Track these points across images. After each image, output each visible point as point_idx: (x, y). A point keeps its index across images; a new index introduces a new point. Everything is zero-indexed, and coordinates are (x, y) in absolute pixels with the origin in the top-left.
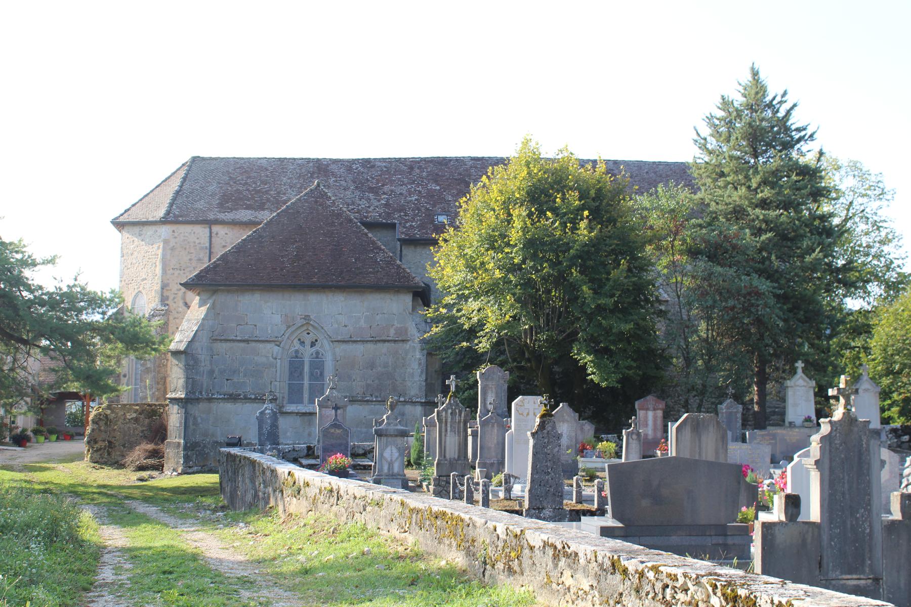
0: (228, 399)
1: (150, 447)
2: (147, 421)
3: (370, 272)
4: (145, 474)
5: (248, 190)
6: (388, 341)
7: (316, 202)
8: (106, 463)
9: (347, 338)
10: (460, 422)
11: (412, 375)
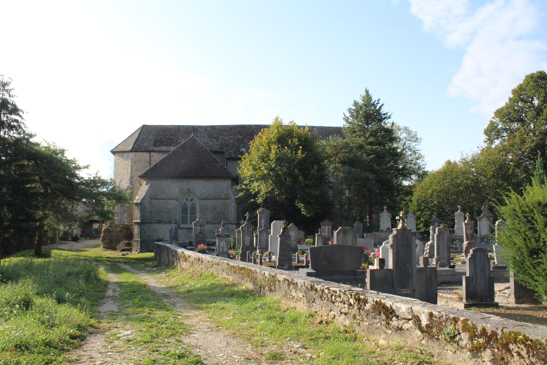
1: (126, 242)
2: (125, 231)
4: (125, 253)
9: (205, 197)
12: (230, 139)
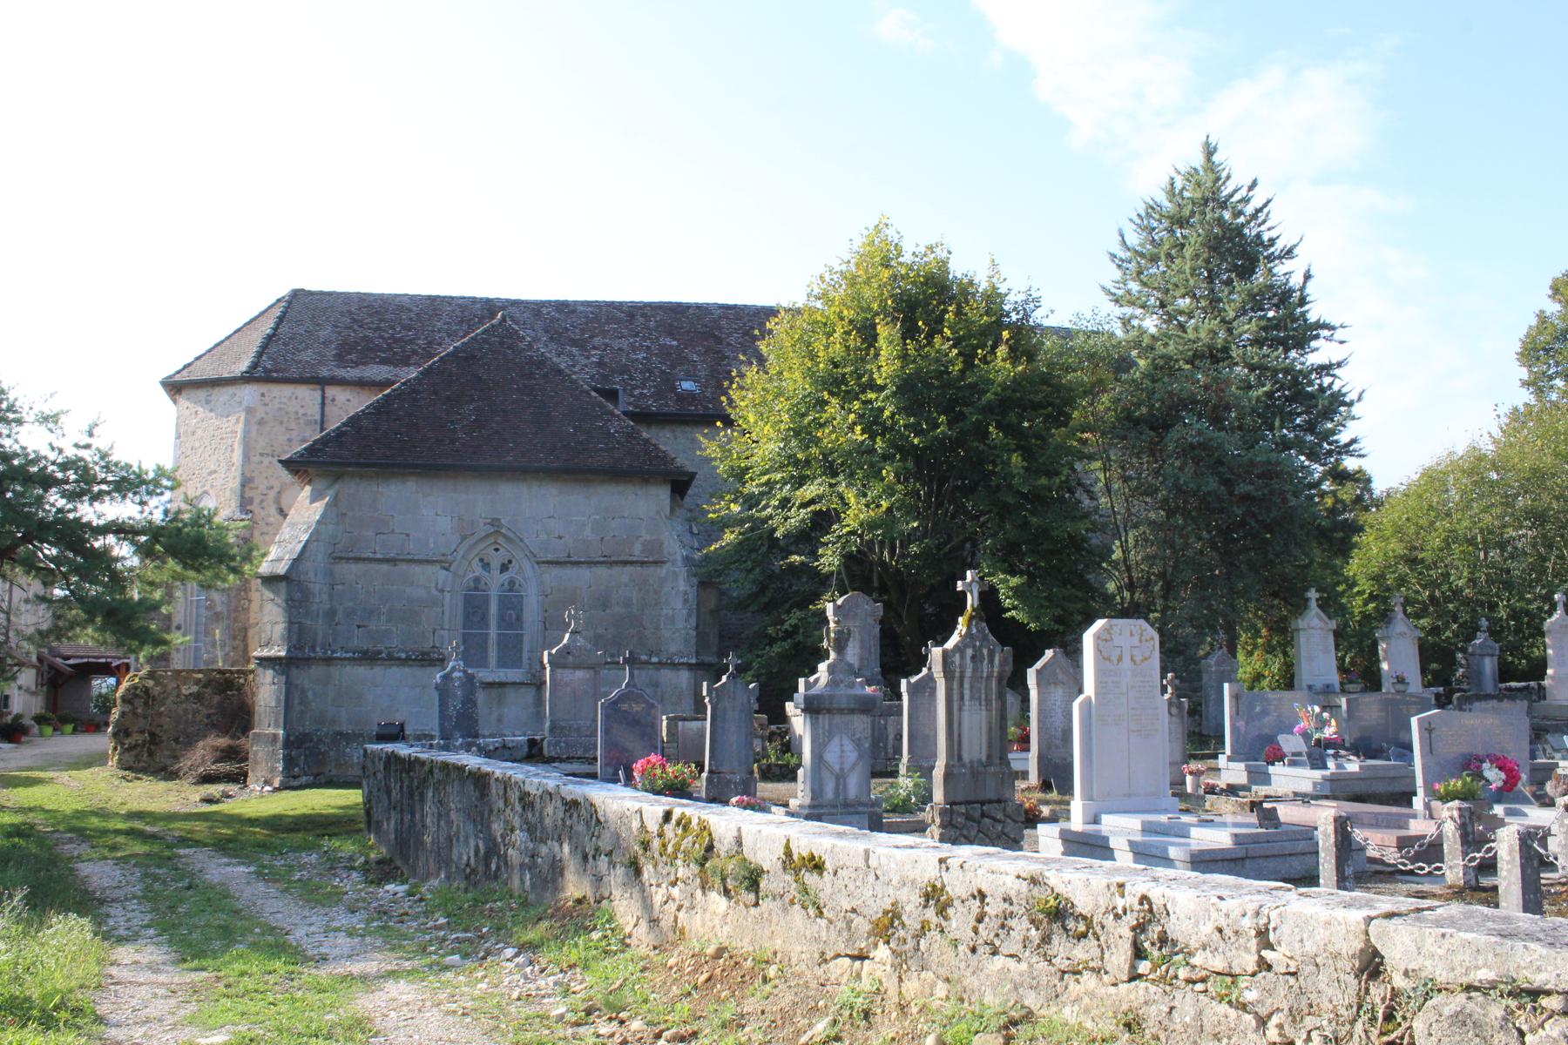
0: (360, 659)
1: (223, 742)
2: (216, 698)
4: (215, 790)
6: (632, 563)
7: (502, 343)
8: (145, 771)
9: (562, 556)
10: (989, 677)
12: (634, 349)
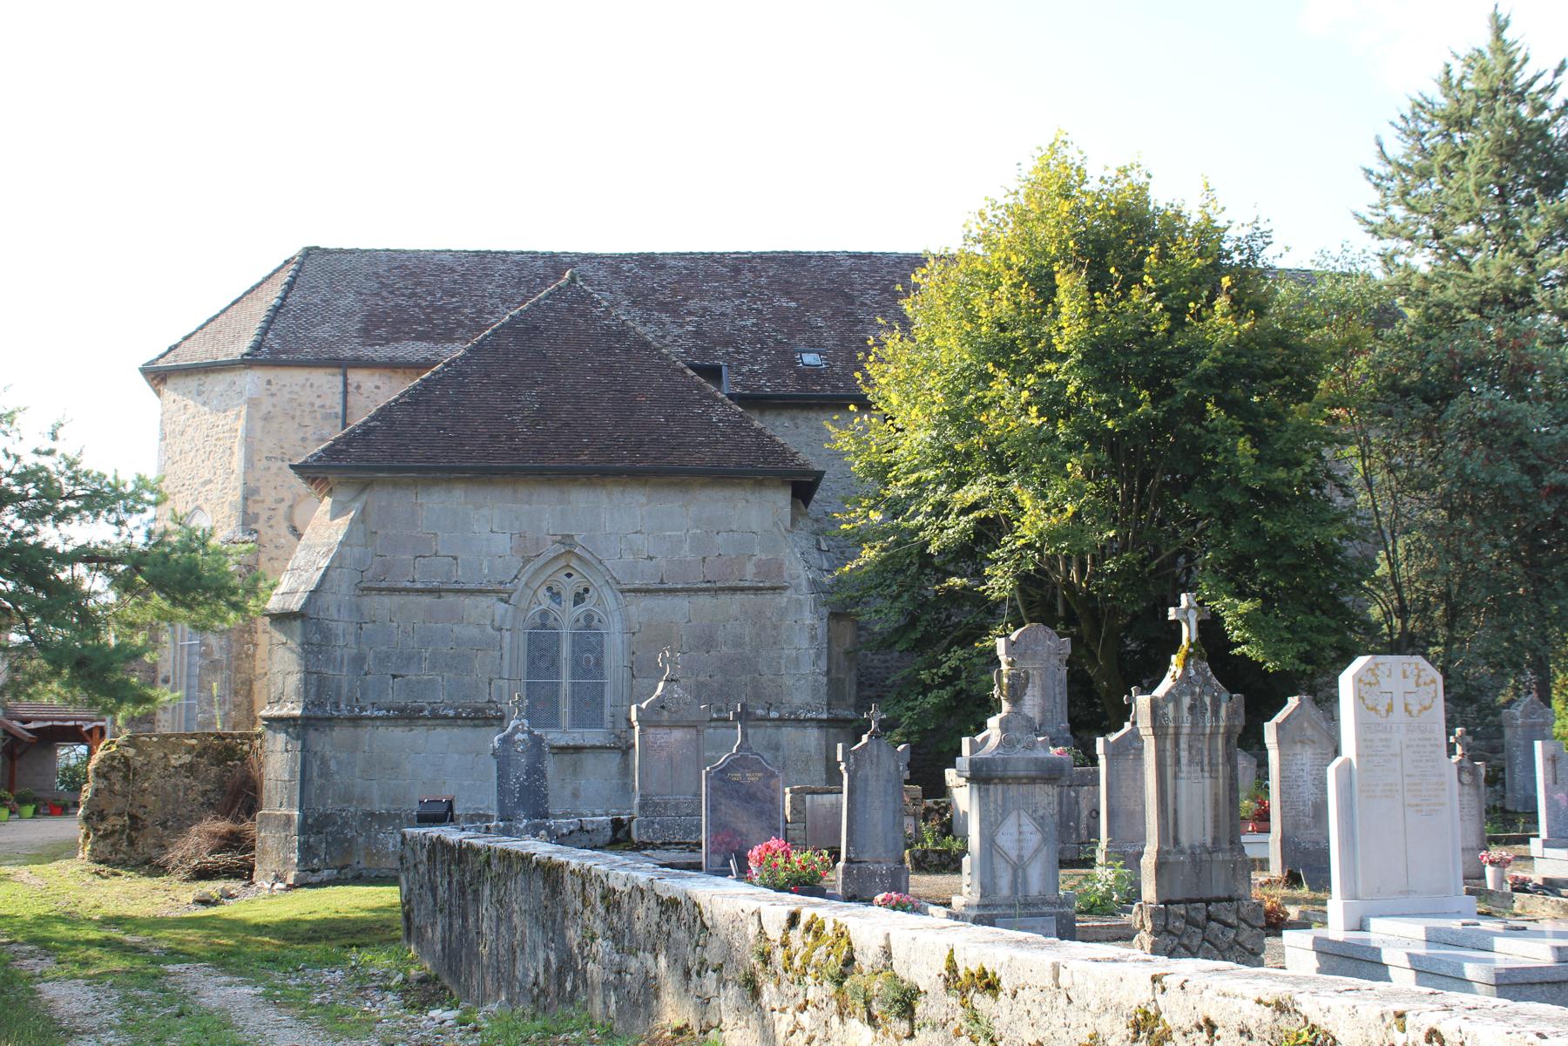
0: (396, 718)
1: (223, 826)
2: (214, 770)
3: (701, 443)
4: (212, 888)
5: (418, 306)
6: (743, 589)
7: (571, 310)
8: (123, 864)
10: (1214, 734)
11: (796, 662)
